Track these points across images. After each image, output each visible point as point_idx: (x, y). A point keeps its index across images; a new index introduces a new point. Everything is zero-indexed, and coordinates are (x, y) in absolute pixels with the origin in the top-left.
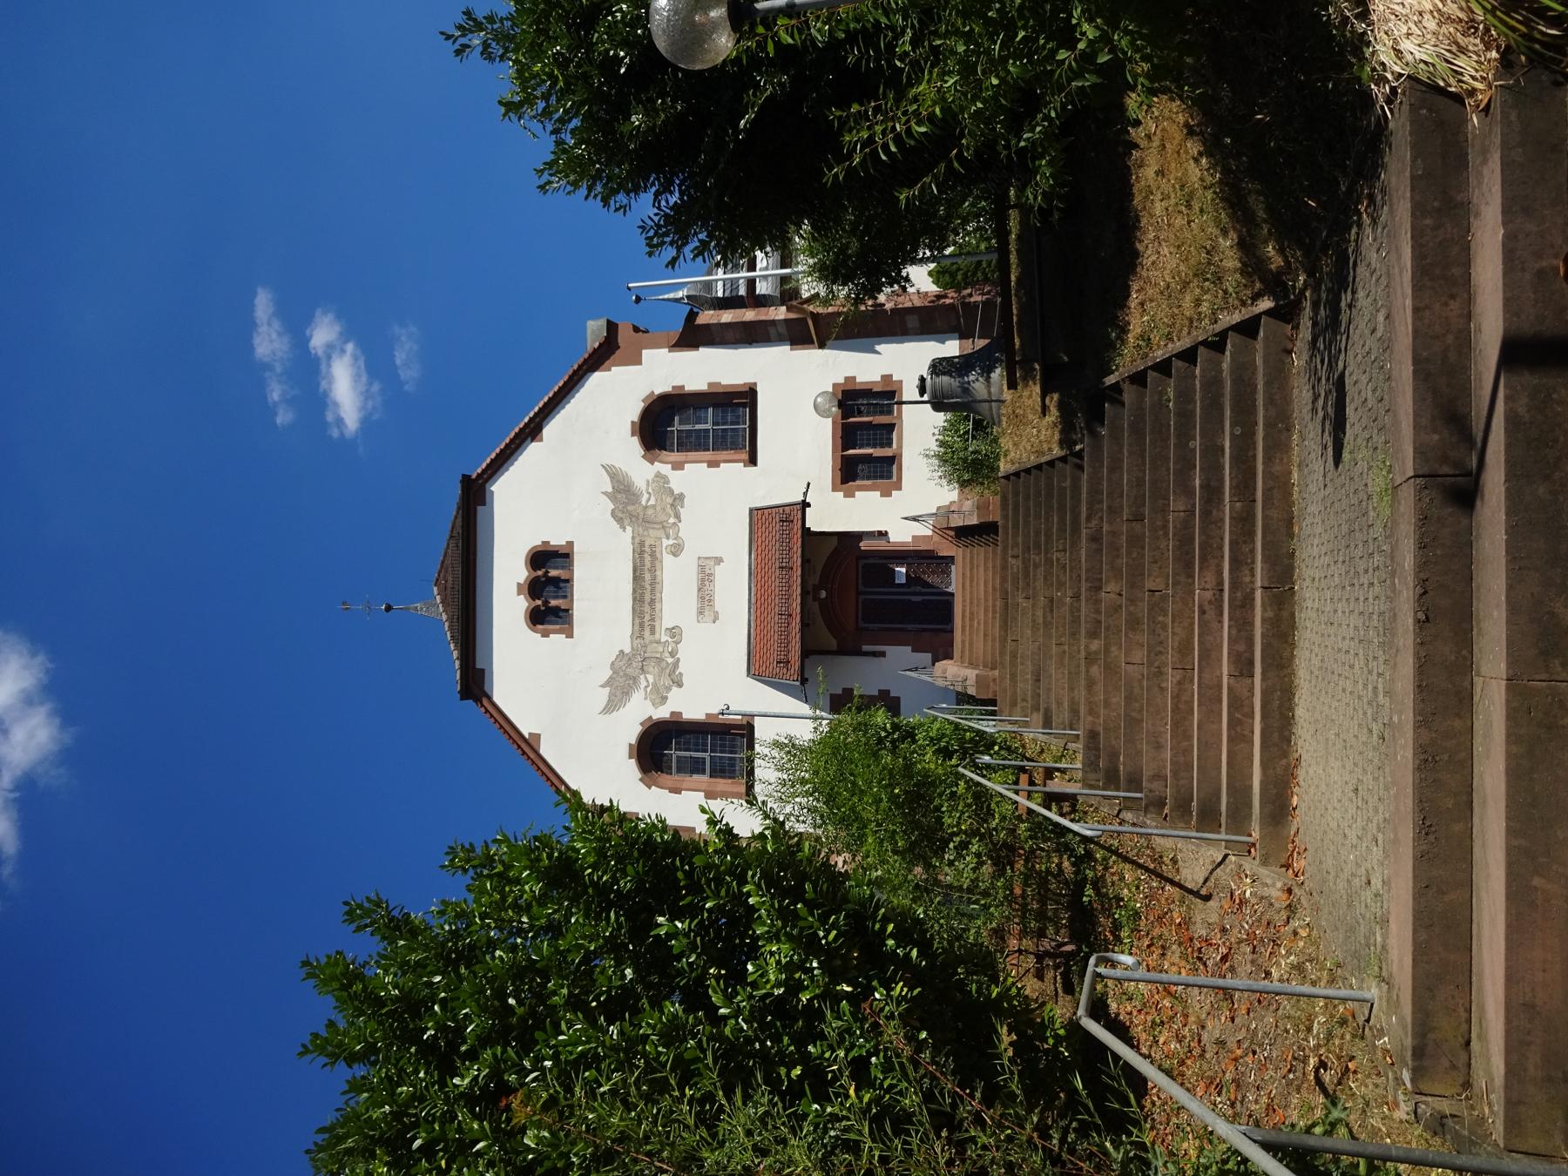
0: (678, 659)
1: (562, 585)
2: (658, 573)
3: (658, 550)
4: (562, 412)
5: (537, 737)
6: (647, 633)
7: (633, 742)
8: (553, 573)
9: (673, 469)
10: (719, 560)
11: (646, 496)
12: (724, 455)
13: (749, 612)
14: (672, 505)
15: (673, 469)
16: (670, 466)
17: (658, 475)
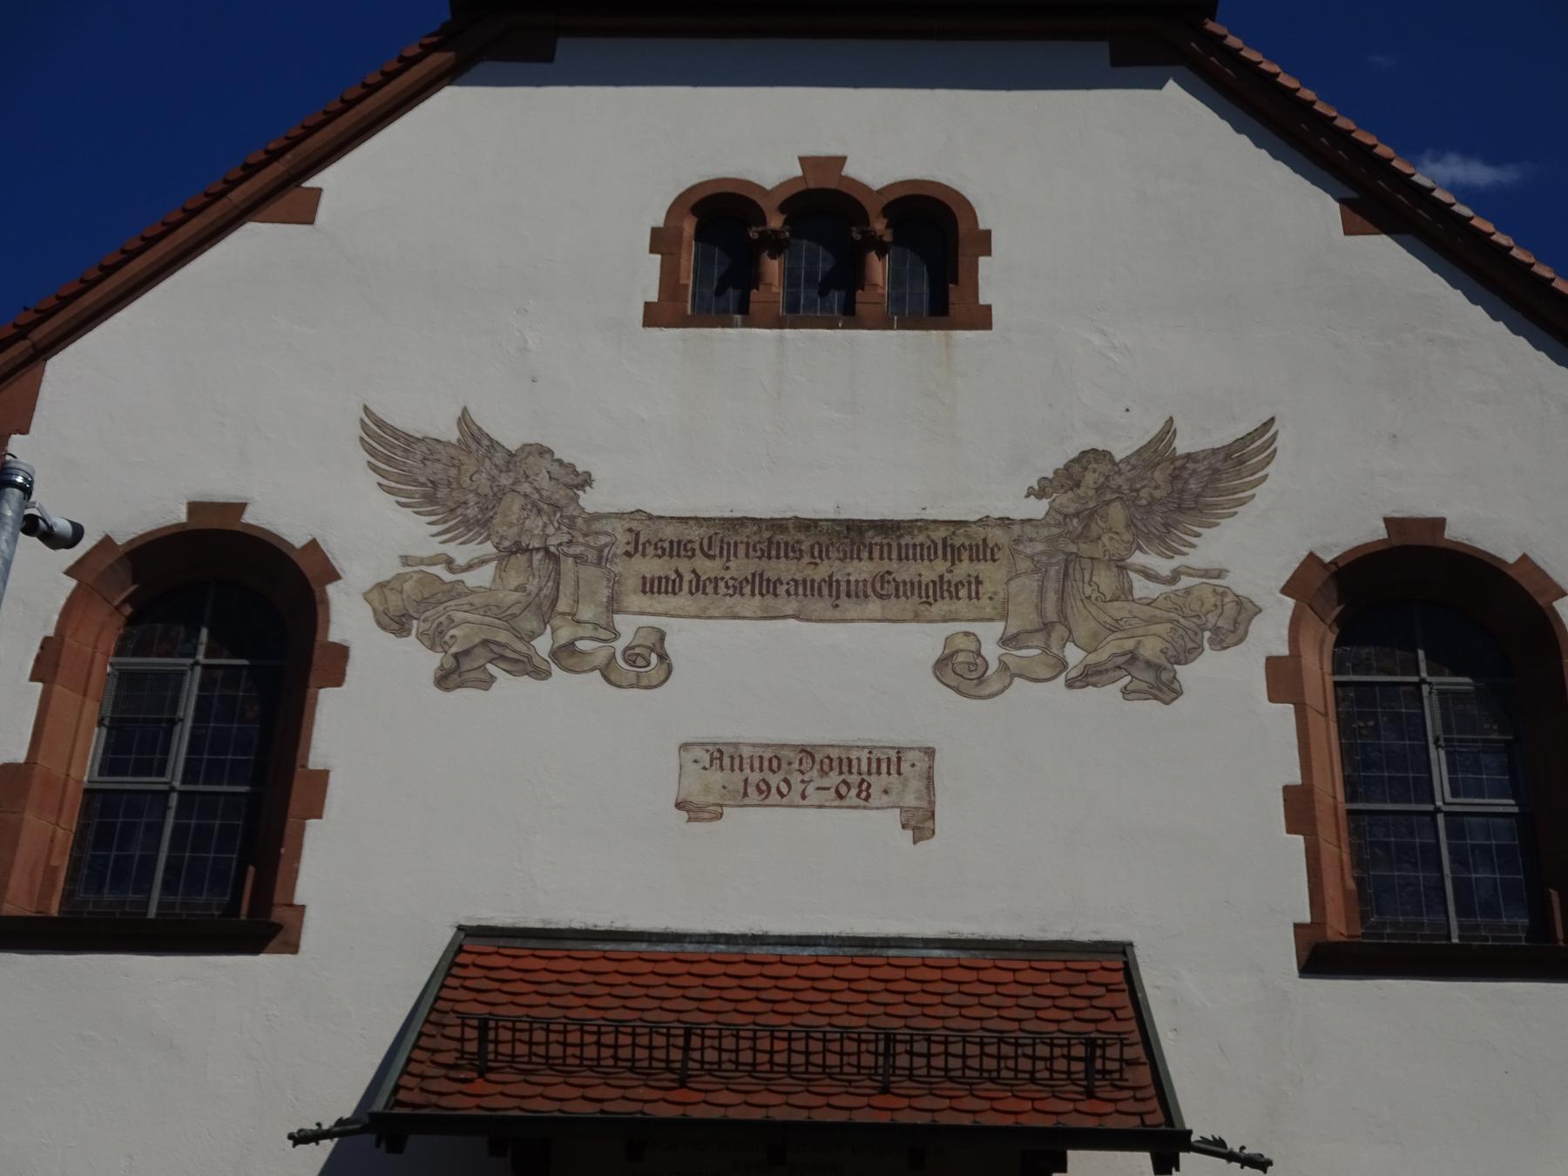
0: (541, 674)
1: (836, 297)
2: (874, 607)
3: (962, 606)
4: (1458, 297)
5: (305, 216)
6: (653, 566)
7: (248, 518)
8: (878, 269)
9: (1273, 663)
10: (920, 824)
11: (1164, 566)
12: (1335, 851)
13: (716, 938)
14: (1133, 657)
15: (1273, 663)
16: (1284, 650)
17: (1244, 612)
